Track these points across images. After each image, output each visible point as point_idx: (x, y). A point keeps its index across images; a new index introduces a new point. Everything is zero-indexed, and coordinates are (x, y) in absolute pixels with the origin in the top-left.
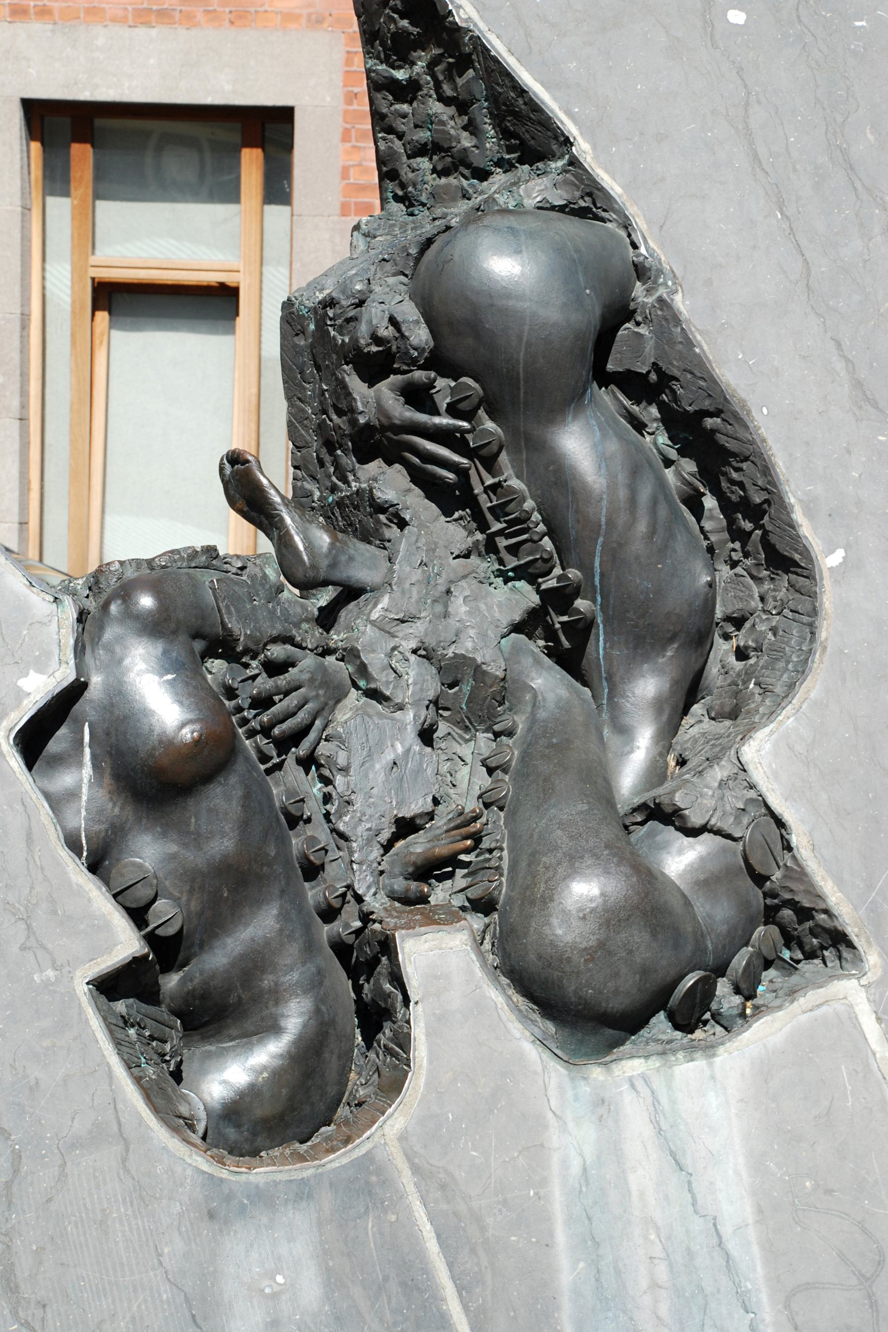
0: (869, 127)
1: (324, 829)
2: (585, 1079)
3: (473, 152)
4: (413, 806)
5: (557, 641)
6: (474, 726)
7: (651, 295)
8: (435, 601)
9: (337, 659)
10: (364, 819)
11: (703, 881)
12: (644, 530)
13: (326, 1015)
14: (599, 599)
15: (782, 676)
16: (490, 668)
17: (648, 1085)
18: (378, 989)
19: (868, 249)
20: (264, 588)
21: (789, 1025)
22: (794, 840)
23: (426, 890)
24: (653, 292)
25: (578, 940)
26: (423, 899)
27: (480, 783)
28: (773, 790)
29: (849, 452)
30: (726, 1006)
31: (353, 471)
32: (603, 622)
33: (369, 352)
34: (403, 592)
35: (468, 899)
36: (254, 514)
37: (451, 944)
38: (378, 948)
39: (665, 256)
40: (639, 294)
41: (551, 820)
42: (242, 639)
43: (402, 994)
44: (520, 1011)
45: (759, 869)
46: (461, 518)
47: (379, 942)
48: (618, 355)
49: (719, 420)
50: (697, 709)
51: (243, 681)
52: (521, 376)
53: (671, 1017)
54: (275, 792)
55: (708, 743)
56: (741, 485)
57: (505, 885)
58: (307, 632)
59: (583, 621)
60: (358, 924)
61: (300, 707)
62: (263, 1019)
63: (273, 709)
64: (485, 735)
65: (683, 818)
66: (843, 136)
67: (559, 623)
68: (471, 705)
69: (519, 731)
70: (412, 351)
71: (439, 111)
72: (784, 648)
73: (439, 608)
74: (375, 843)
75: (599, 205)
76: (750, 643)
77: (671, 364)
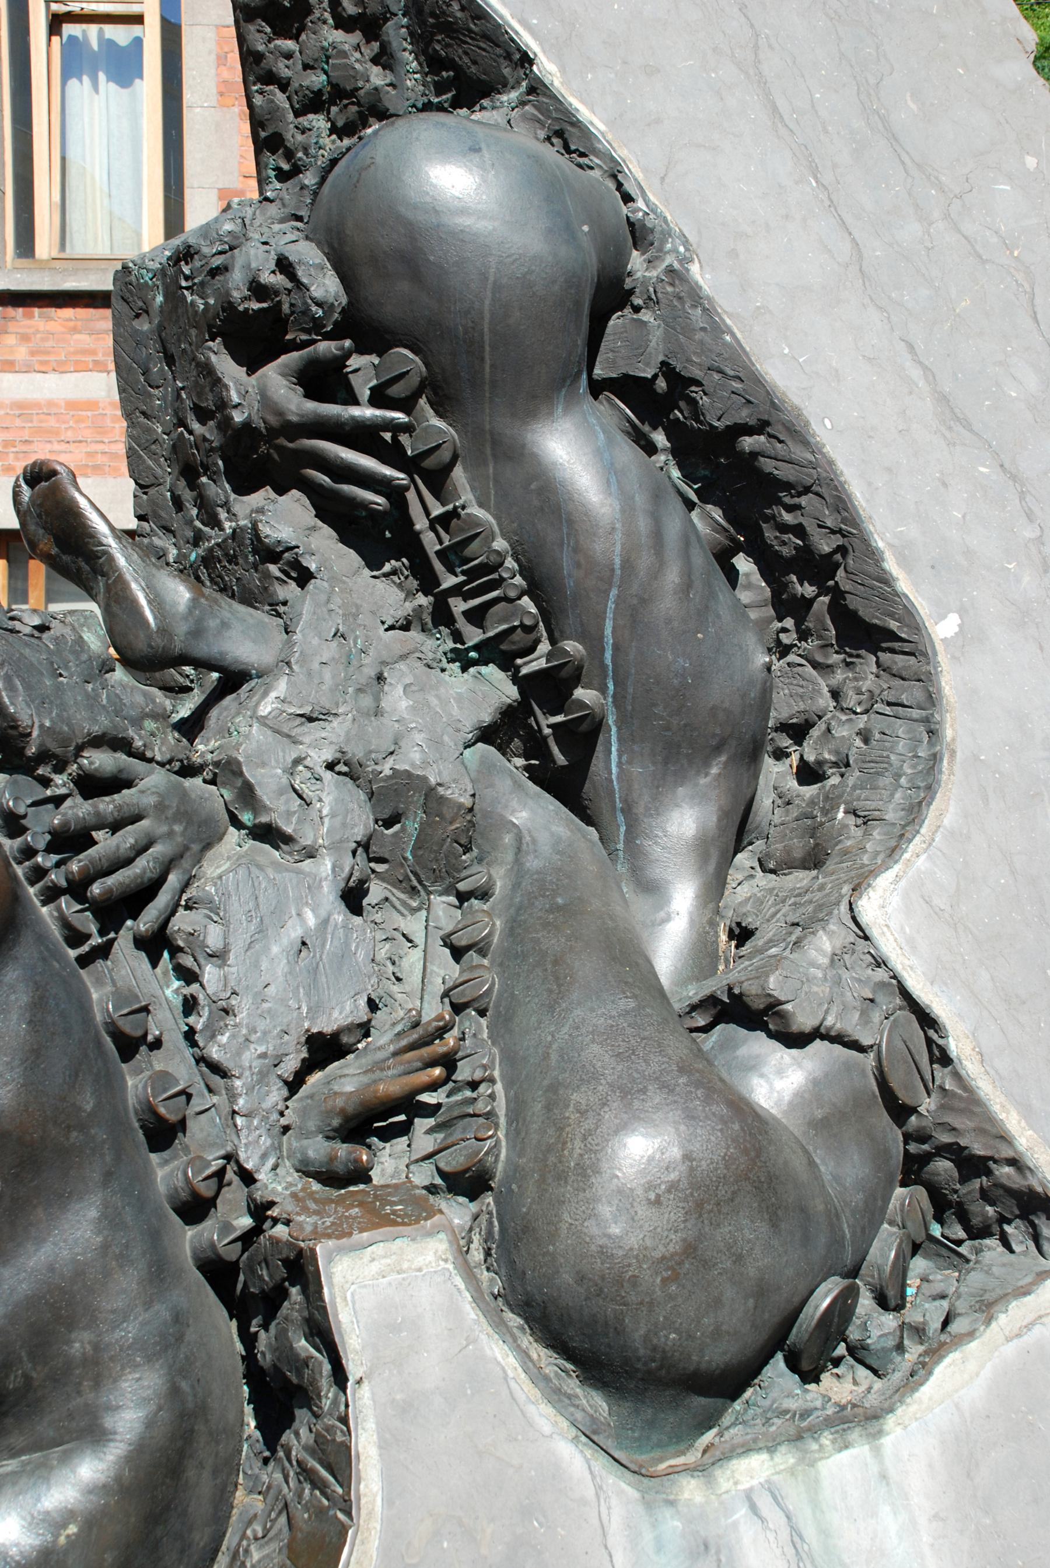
0: (908, 94)
1: (183, 1059)
2: (672, 1503)
3: (388, 93)
4: (336, 1014)
5: (545, 755)
6: (424, 887)
7: (654, 268)
8: (360, 690)
9: (205, 781)
10: (253, 1038)
11: (822, 1120)
12: (677, 580)
13: (190, 1398)
14: (611, 686)
15: (892, 795)
16: (449, 792)
17: (778, 1504)
18: (284, 1348)
19: (929, 235)
20: (78, 658)
21: (989, 1365)
22: (954, 1047)
23: (365, 1158)
24: (656, 263)
25: (649, 1243)
26: (361, 1175)
27: (442, 973)
28: (911, 968)
29: (945, 485)
30: (875, 1333)
31: (226, 505)
32: (616, 722)
33: (247, 310)
34: (309, 674)
35: (440, 1172)
36: (67, 558)
37: (420, 1261)
38: (283, 1272)
39: (671, 215)
40: (637, 266)
41: (577, 1028)
42: (35, 733)
43: (330, 1362)
44: (546, 1378)
45: (904, 1097)
46: (394, 572)
47: (286, 1262)
48: (610, 355)
49: (762, 438)
50: (744, 859)
51: (35, 804)
52: (487, 338)
53: (793, 1364)
54: (95, 996)
55: (783, 901)
56: (799, 530)
57: (504, 1143)
58: (153, 734)
59: (588, 721)
60: (246, 1222)
61: (141, 850)
62: (71, 1416)
63: (90, 851)
64: (444, 898)
65: (782, 1016)
66: (879, 99)
67: (549, 726)
68: (421, 852)
69: (499, 887)
70: (314, 308)
71: (338, 40)
72: (888, 757)
73: (367, 701)
74: (273, 1079)
75: (573, 147)
76: (827, 756)
77: (689, 360)
